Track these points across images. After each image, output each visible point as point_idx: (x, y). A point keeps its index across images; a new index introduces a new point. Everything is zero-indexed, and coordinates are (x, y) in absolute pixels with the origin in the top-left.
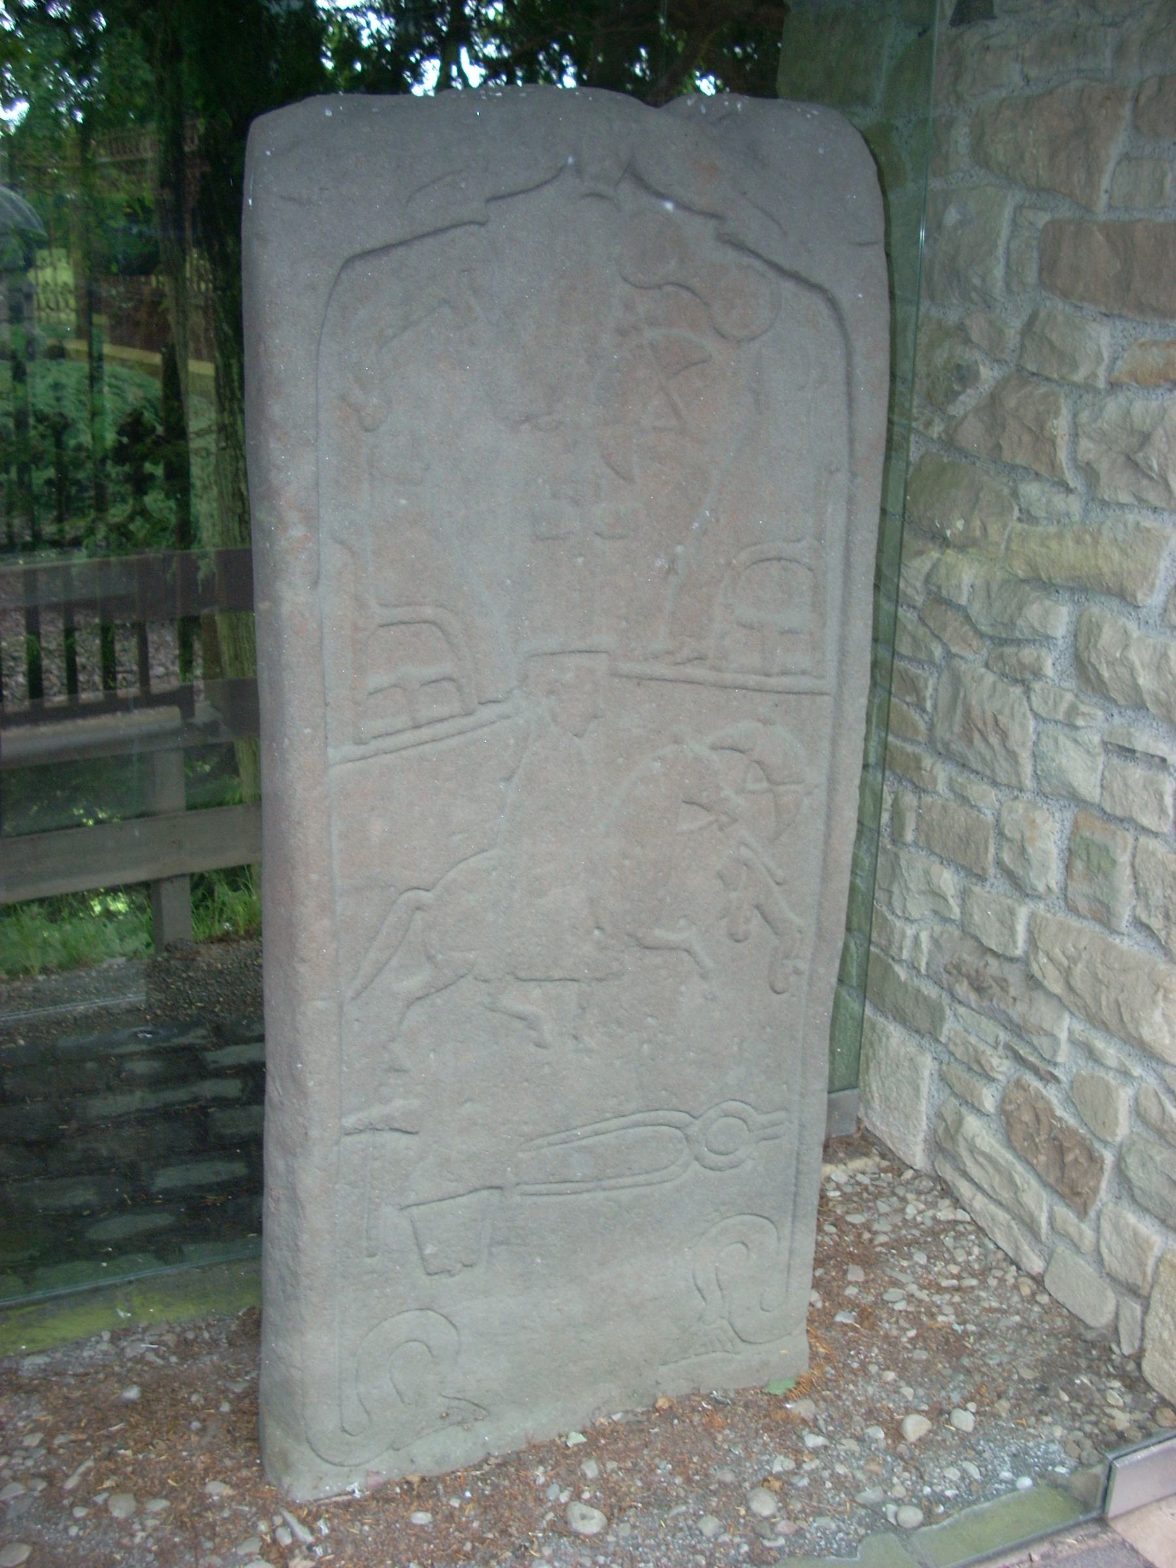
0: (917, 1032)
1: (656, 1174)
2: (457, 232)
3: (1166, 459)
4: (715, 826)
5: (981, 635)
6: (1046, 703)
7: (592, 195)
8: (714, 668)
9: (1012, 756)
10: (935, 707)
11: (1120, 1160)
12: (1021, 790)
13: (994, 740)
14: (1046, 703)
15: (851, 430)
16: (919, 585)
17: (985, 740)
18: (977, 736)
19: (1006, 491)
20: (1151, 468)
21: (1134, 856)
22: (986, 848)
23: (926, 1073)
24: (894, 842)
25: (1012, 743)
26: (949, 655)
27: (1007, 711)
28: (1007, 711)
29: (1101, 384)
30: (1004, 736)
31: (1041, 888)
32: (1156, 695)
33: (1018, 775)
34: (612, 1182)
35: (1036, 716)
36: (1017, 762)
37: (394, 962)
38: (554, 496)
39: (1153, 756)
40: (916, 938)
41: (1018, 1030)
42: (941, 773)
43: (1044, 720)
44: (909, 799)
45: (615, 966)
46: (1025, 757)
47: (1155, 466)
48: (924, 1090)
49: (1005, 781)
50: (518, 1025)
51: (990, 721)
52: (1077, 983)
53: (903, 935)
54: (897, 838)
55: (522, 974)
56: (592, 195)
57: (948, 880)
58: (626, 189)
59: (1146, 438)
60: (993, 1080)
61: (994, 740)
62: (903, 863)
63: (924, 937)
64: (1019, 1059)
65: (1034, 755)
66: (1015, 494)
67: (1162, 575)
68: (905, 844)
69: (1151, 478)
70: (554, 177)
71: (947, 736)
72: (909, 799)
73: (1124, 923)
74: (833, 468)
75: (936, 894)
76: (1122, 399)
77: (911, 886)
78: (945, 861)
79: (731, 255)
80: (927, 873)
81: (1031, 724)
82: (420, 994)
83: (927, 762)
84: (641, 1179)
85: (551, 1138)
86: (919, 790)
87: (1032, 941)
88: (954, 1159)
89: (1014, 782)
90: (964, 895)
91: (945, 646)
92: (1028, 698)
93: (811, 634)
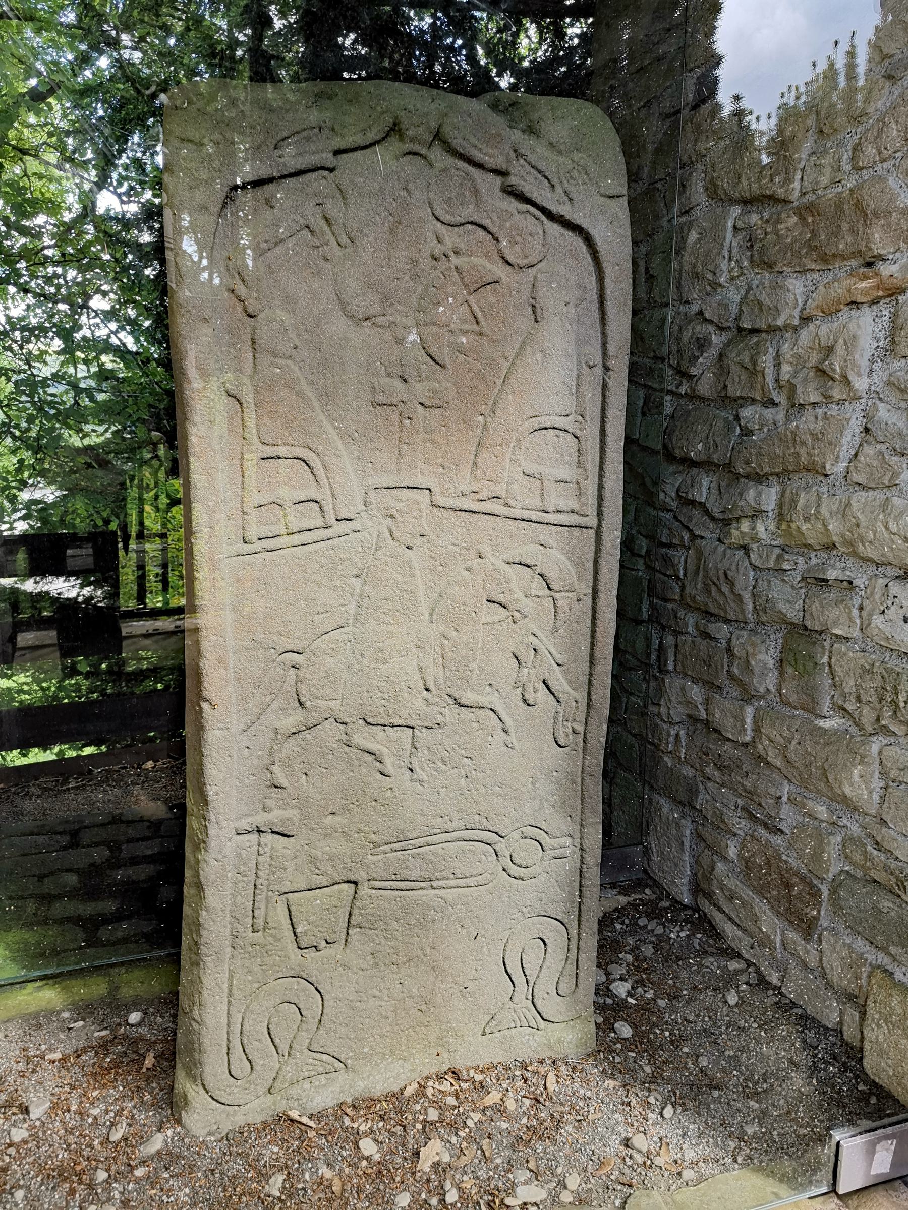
0: (680, 802)
1: (473, 879)
2: (313, 176)
3: (846, 361)
4: (510, 619)
5: (713, 519)
6: (761, 557)
7: (409, 153)
8: (506, 505)
9: (739, 598)
10: (685, 575)
11: (833, 891)
12: (746, 623)
13: (725, 589)
14: (761, 557)
15: (604, 334)
16: (673, 494)
17: (719, 590)
18: (713, 589)
19: (731, 418)
20: (834, 370)
21: (830, 658)
22: (723, 667)
23: (688, 832)
24: (661, 671)
25: (738, 589)
26: (694, 537)
27: (733, 567)
28: (733, 567)
29: (796, 322)
30: (732, 584)
31: (762, 690)
32: (843, 536)
33: (743, 611)
34: (440, 883)
35: (755, 568)
36: (742, 602)
37: (275, 705)
38: (389, 375)
39: (842, 581)
40: (677, 735)
41: (750, 794)
42: (691, 621)
43: (760, 569)
44: (669, 640)
45: (439, 719)
46: (747, 596)
47: (838, 368)
48: (687, 845)
49: (734, 618)
50: (370, 758)
51: (721, 573)
52: (792, 756)
53: (669, 735)
54: (663, 670)
55: (370, 720)
56: (409, 153)
57: (696, 693)
58: (437, 154)
59: (829, 350)
60: (735, 835)
61: (725, 589)
62: (667, 685)
63: (682, 732)
64: (752, 817)
65: (753, 595)
66: (737, 418)
67: (845, 448)
68: (668, 671)
69: (833, 379)
70: (383, 139)
71: (694, 592)
72: (669, 640)
73: (826, 709)
74: (591, 364)
75: (689, 703)
76: (812, 326)
77: (673, 699)
78: (695, 680)
79: (514, 205)
80: (683, 689)
81: (752, 574)
82: (294, 730)
83: (681, 614)
84: (462, 882)
85: (395, 846)
86: (676, 633)
87: (757, 730)
88: (709, 896)
89: (740, 617)
90: (707, 702)
91: (691, 531)
92: (749, 557)
93: (578, 483)
